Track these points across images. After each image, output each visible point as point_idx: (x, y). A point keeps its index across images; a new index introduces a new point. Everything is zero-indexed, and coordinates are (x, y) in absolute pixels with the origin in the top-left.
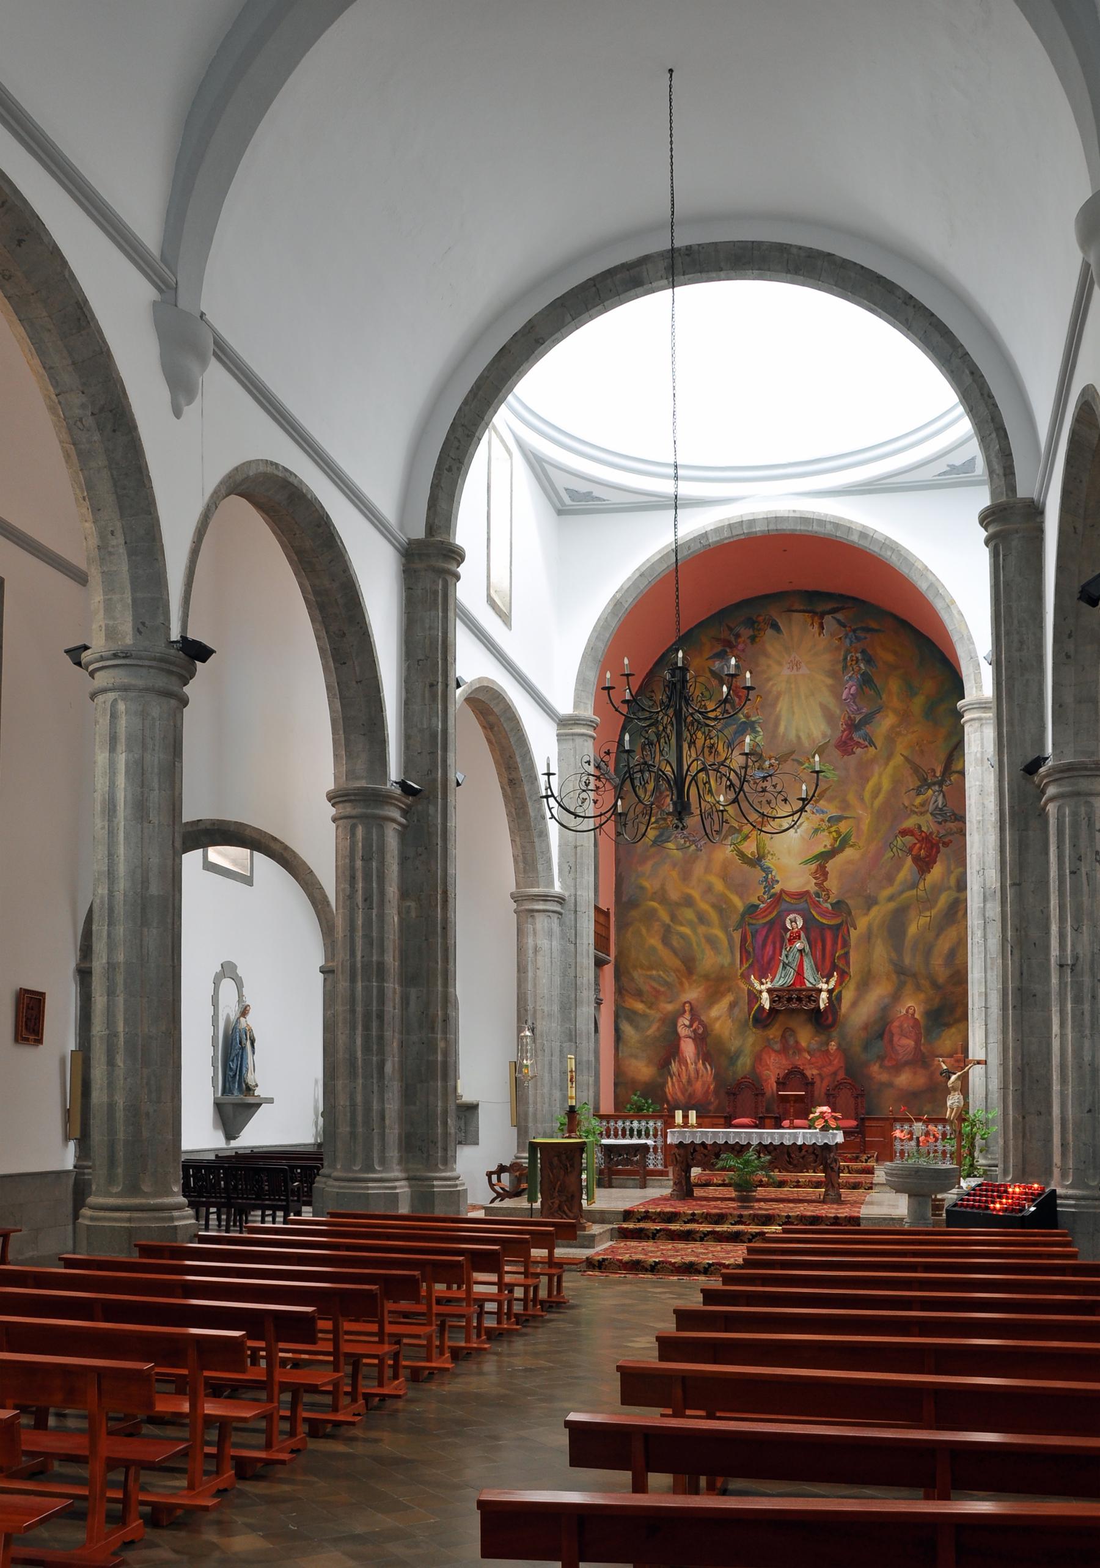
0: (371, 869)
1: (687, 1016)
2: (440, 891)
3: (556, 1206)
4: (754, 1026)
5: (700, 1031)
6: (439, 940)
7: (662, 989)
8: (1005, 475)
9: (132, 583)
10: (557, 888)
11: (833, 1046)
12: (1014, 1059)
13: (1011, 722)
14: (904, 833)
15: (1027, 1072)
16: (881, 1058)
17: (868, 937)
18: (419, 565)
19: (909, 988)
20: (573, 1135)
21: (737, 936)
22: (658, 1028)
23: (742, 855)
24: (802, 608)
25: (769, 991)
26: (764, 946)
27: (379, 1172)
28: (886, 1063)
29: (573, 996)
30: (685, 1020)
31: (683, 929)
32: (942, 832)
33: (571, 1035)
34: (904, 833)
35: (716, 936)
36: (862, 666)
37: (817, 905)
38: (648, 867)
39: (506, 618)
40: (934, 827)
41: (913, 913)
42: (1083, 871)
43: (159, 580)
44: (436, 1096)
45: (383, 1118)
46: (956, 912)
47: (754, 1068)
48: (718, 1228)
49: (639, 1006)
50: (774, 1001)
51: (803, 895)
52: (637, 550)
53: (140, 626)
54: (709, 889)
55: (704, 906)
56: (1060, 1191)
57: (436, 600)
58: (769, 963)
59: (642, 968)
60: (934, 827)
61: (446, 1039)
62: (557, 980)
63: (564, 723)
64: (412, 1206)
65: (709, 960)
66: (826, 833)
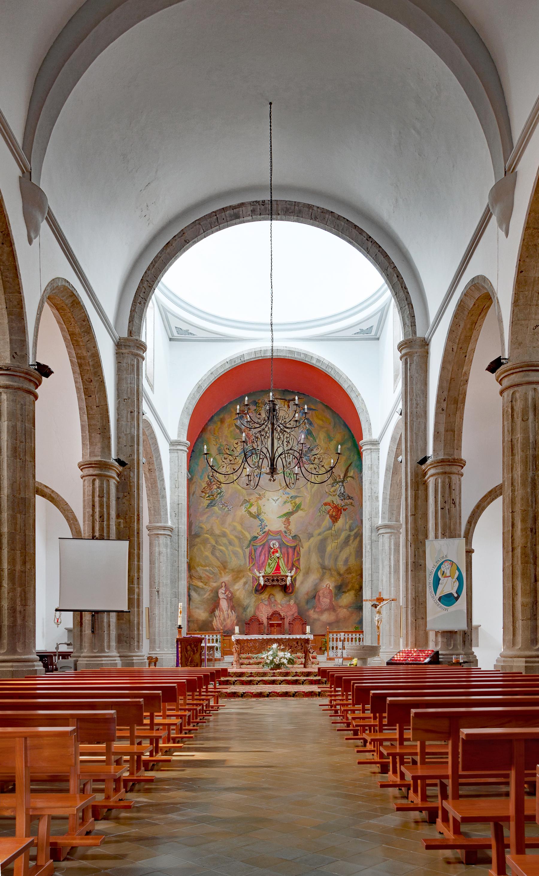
0: (103, 501)
1: (223, 588)
4: (255, 593)
5: (230, 596)
6: (136, 539)
7: (211, 576)
9: (10, 330)
10: (170, 524)
12: (412, 594)
13: (412, 441)
14: (326, 504)
15: (417, 600)
16: (314, 608)
18: (124, 351)
19: (327, 575)
21: (247, 551)
22: (209, 595)
23: (250, 513)
24: (279, 397)
26: (260, 556)
27: (108, 652)
28: (317, 610)
30: (222, 591)
31: (221, 547)
32: (343, 504)
33: (176, 595)
34: (326, 504)
36: (307, 426)
38: (204, 518)
41: (329, 541)
42: (447, 508)
43: (23, 330)
44: (134, 615)
45: (109, 626)
46: (349, 541)
47: (255, 613)
48: (264, 678)
49: (200, 584)
50: (266, 581)
51: (278, 532)
53: (14, 354)
54: (235, 529)
57: (133, 369)
58: (262, 564)
59: (202, 566)
61: (139, 587)
62: (169, 568)
63: (173, 444)
65: (234, 563)
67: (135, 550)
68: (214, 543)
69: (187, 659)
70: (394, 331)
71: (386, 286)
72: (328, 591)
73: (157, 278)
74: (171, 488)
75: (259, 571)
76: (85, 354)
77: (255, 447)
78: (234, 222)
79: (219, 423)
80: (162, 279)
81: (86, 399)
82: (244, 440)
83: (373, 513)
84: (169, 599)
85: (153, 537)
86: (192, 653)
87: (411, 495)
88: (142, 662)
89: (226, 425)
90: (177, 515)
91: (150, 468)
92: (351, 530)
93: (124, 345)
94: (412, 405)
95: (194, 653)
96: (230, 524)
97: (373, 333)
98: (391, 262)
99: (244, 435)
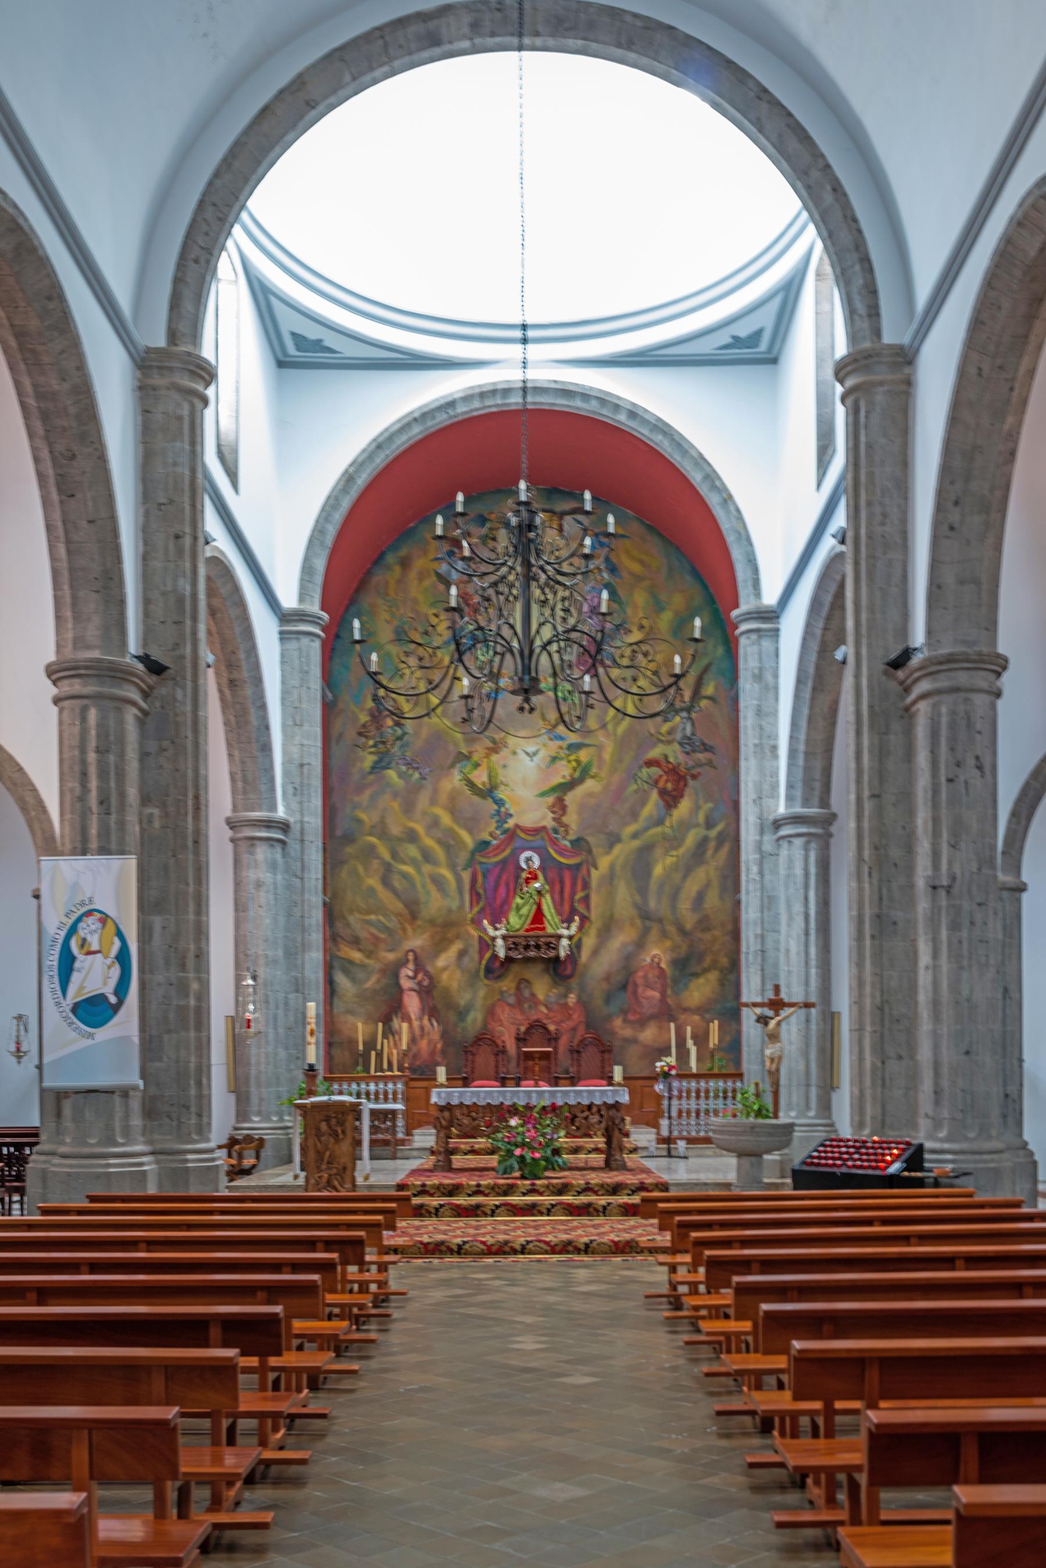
1: (411, 966)
2: (190, 795)
3: (324, 1180)
4: (486, 977)
7: (382, 936)
8: (870, 316)
10: (281, 812)
11: (572, 999)
12: (873, 996)
13: (871, 609)
14: (650, 763)
15: (887, 1010)
16: (624, 1012)
17: (611, 877)
18: (157, 380)
21: (466, 876)
22: (378, 981)
23: (471, 784)
25: (504, 938)
27: (123, 1145)
29: (299, 939)
30: (408, 971)
32: (691, 763)
33: (297, 985)
34: (650, 763)
35: (444, 877)
37: (554, 842)
38: (365, 797)
39: (233, 476)
40: (682, 758)
41: (658, 852)
46: (704, 852)
47: (485, 1024)
49: (357, 956)
50: (510, 949)
52: (374, 413)
54: (435, 823)
55: (429, 842)
56: (928, 1145)
58: (502, 906)
59: (360, 912)
60: (682, 758)
62: (282, 920)
63: (285, 617)
64: (160, 1186)
65: (435, 904)
66: (564, 762)
67: (187, 884)
68: (387, 857)
69: (320, 1155)
70: (819, 333)
71: (805, 215)
72: (656, 972)
73: (237, 198)
74: (284, 726)
75: (492, 924)
76: (56, 387)
77: (483, 623)
78: (425, 54)
79: (398, 569)
80: (251, 203)
81: (61, 502)
82: (453, 603)
83: (766, 787)
84: (281, 996)
85: (243, 839)
86: (332, 1140)
87: (871, 745)
88: (208, 1167)
89: (413, 575)
90: (297, 790)
91: (232, 677)
92: (709, 825)
93: (160, 368)
94: (870, 517)
95: (337, 1140)
96: (423, 822)
97: (763, 346)
98: (817, 154)
99: (454, 591)
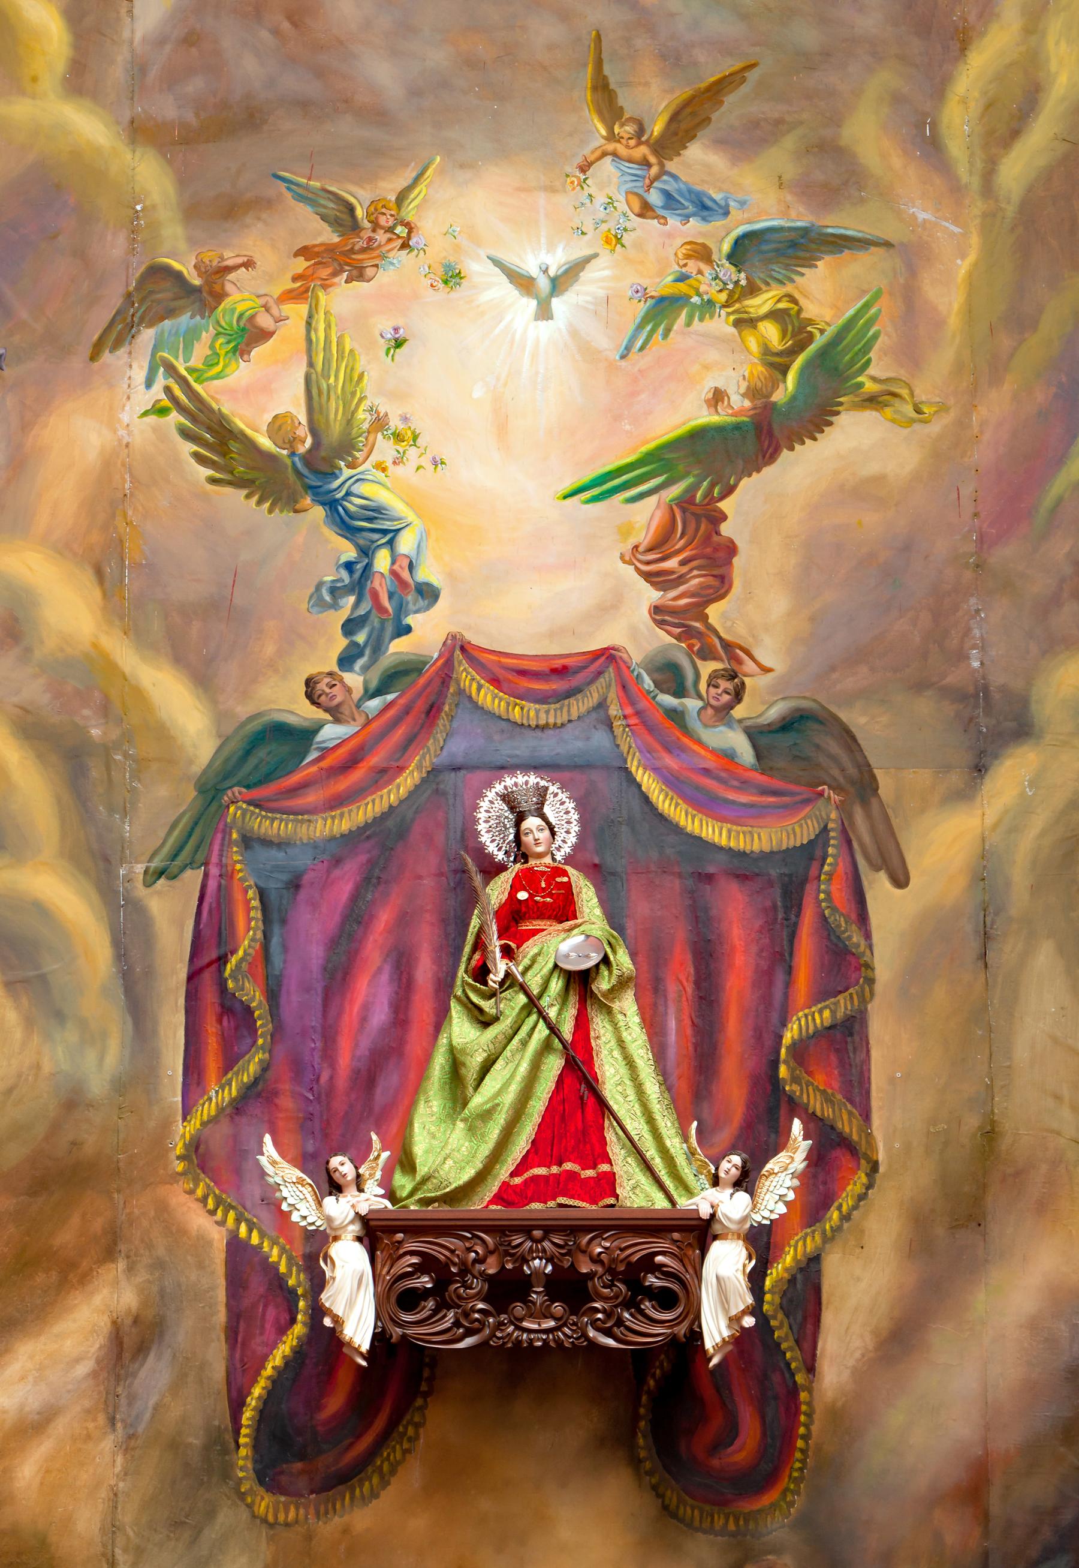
20: (244, 966)
21: (170, 915)
23: (216, 437)
26: (338, 978)
35: (41, 910)
37: (666, 732)
50: (409, 1300)
58: (366, 1080)
66: (721, 324)
